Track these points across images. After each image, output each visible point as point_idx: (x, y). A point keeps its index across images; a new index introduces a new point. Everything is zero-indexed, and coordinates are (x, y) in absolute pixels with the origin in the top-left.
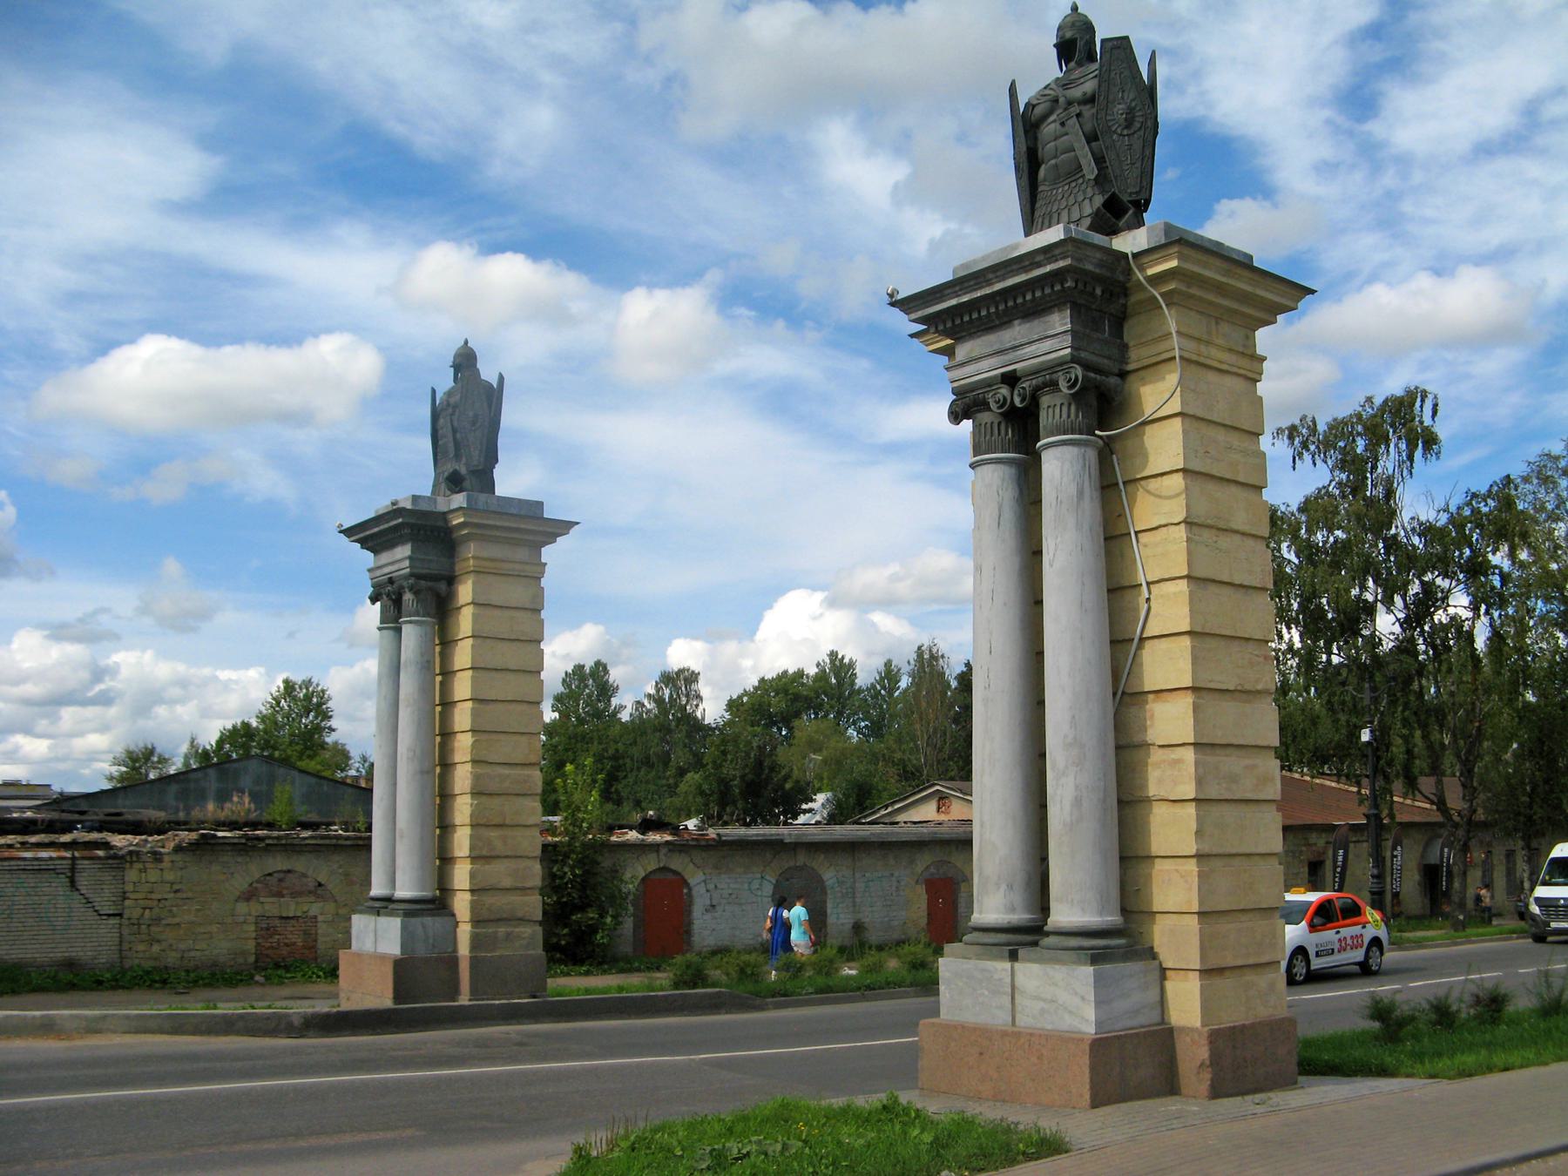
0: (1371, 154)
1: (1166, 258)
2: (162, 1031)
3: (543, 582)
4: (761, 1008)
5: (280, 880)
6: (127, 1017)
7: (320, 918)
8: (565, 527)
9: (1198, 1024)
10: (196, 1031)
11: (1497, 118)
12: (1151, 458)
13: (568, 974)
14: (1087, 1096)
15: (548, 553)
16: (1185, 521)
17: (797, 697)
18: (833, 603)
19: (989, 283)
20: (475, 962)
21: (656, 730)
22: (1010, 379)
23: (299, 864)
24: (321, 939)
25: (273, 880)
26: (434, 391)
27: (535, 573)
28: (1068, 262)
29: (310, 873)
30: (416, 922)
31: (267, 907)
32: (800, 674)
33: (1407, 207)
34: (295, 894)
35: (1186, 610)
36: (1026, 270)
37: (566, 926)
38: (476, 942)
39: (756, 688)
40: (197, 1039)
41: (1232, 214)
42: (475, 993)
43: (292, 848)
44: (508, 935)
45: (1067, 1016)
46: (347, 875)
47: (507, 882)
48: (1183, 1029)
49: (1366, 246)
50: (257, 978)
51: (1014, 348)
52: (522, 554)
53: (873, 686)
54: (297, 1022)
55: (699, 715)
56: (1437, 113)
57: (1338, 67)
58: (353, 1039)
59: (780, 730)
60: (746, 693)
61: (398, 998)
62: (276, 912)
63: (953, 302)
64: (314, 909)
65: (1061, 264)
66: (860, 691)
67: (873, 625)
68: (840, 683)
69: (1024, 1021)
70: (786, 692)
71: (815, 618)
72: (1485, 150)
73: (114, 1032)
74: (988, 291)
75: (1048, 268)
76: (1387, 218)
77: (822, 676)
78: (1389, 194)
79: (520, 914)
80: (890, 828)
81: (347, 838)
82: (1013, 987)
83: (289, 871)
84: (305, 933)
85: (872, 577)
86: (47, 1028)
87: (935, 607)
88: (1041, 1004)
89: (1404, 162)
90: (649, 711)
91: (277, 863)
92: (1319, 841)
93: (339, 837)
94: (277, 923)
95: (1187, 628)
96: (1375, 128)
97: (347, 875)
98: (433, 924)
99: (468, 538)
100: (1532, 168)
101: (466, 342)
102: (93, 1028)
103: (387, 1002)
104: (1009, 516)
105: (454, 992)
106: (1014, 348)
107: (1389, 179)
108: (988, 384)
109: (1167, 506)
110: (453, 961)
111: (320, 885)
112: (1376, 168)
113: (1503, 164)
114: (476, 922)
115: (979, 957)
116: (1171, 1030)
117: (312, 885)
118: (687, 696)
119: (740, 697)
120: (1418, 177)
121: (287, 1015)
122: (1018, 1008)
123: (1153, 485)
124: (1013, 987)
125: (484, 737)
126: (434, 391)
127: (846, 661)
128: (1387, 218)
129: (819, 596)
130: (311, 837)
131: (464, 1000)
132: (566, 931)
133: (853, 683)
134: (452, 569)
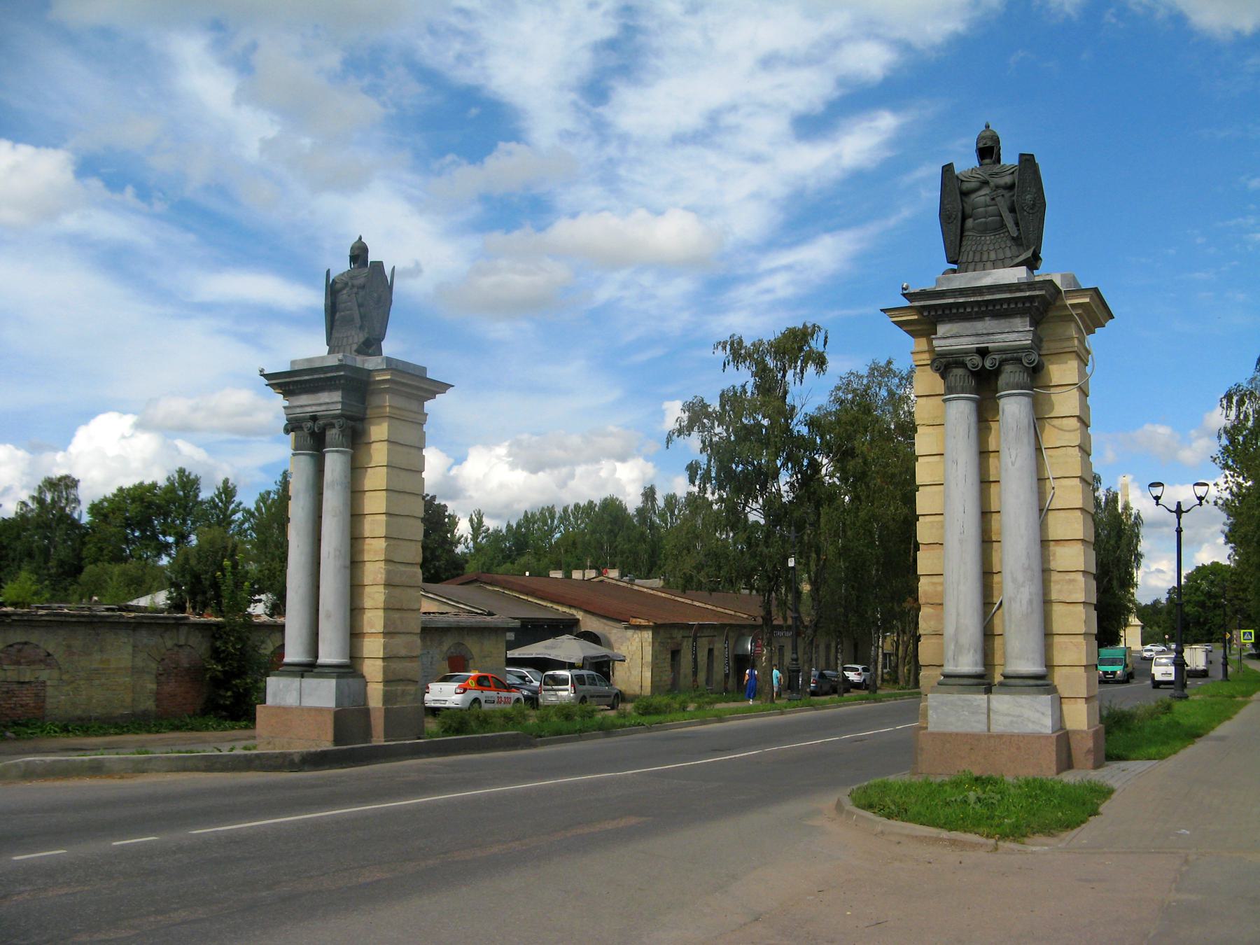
0: (601, 130)
1: (1082, 296)
2: (198, 770)
3: (425, 428)
4: (535, 746)
5: (20, 651)
6: (169, 758)
7: (49, 683)
8: (443, 387)
9: (1085, 728)
10: (225, 769)
11: (690, 119)
12: (1056, 407)
13: (233, 728)
14: (1055, 769)
15: (429, 405)
16: (1079, 446)
17: (150, 505)
18: (141, 426)
19: (993, 294)
20: (388, 713)
21: (38, 526)
22: (983, 352)
23: (35, 637)
24: (48, 700)
25: (13, 650)
26: (328, 272)
27: (419, 420)
28: (1043, 292)
29: (42, 645)
30: (344, 681)
31: (9, 674)
32: (154, 485)
33: (622, 171)
34: (30, 663)
35: (1080, 496)
36: (1011, 291)
37: (227, 690)
38: (388, 698)
39: (115, 495)
40: (229, 775)
41: (510, 153)
42: (388, 735)
43: (30, 623)
44: (403, 691)
45: (1030, 725)
46: (69, 646)
47: (403, 652)
48: (1075, 732)
49: (591, 192)
50: (8, 734)
51: (988, 334)
52: (413, 406)
53: (213, 500)
54: (297, 759)
55: (76, 516)
56: (649, 108)
57: (585, 61)
58: (57, 783)
59: (133, 531)
60: (105, 499)
61: (337, 741)
62: (15, 678)
63: (951, 301)
64: (44, 674)
65: (1038, 293)
66: (202, 503)
67: (177, 449)
68: (186, 496)
69: (996, 728)
70: (142, 500)
71: (124, 437)
72: (681, 139)
73: (158, 771)
74: (979, 299)
75: (1028, 294)
76: (608, 178)
77: (171, 489)
78: (610, 160)
79: (409, 677)
80: (489, 618)
81: (73, 616)
82: (989, 710)
83: (26, 643)
84: (37, 695)
85: (177, 407)
86: (96, 769)
87: (225, 436)
88: (1010, 718)
89: (624, 139)
90: (32, 510)
91: (17, 636)
92: (678, 635)
93: (66, 615)
94: (15, 687)
95: (1080, 506)
96: (604, 111)
97: (69, 646)
98: (352, 682)
99: (386, 391)
100: (712, 157)
101: (360, 238)
102: (139, 769)
103: (327, 744)
104: (973, 432)
105: (367, 734)
106: (988, 334)
107: (612, 150)
108: (966, 352)
109: (1068, 436)
110: (366, 712)
111: (49, 655)
112: (604, 140)
113: (690, 150)
114: (387, 682)
115: (959, 692)
116: (1067, 732)
117: (43, 654)
118: (67, 499)
119: (101, 502)
120: (632, 152)
121: (291, 754)
122: (992, 722)
123: (1056, 422)
124: (989, 710)
125: (392, 542)
126: (328, 272)
127: (192, 477)
128: (608, 178)
129: (130, 419)
130: (47, 615)
131: (378, 739)
132: (229, 693)
133: (197, 496)
134: (365, 414)
